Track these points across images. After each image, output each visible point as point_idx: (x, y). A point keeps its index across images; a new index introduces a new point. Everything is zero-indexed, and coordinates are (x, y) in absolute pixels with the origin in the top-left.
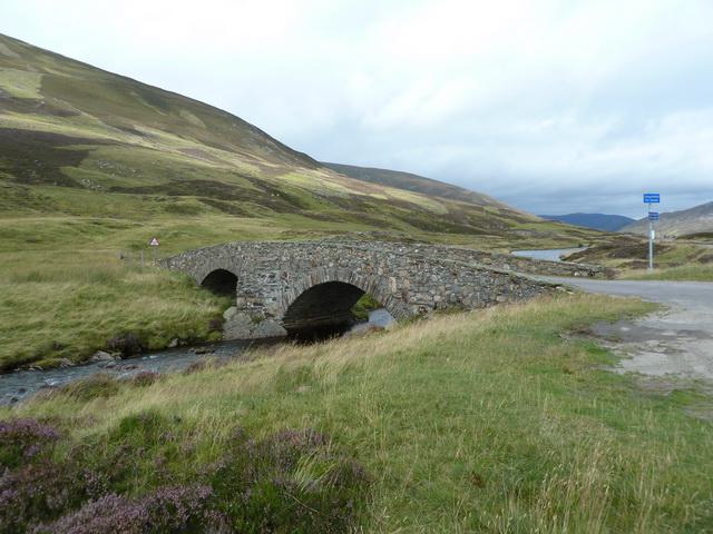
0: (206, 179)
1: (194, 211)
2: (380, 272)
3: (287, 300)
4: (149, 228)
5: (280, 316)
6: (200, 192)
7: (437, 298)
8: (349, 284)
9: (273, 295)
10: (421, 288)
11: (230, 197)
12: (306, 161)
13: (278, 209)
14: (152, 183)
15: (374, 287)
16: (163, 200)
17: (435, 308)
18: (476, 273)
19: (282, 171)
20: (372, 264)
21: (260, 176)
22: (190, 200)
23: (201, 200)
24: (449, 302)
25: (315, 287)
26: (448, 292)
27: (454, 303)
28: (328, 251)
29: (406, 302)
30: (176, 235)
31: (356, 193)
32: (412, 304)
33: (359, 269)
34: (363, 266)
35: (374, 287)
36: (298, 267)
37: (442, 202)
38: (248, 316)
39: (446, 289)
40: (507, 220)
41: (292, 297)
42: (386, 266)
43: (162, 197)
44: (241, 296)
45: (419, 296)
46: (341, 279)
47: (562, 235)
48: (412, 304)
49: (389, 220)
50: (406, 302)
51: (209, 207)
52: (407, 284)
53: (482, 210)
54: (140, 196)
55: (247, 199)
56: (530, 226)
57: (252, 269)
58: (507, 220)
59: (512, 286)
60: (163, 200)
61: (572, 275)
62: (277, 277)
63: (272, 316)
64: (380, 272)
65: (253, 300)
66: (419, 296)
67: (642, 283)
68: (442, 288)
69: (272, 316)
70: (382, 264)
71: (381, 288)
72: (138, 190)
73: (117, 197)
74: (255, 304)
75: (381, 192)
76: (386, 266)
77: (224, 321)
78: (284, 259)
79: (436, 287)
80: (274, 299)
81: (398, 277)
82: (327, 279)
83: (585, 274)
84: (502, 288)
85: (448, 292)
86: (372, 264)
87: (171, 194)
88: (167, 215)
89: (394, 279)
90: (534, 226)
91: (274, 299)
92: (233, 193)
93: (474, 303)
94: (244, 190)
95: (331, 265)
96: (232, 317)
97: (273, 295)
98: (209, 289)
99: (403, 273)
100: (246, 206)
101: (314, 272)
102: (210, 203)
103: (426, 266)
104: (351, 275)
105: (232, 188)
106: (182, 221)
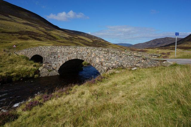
0: (30, 31)
1: (27, 39)
2: (93, 56)
3: (60, 65)
4: (14, 43)
5: (58, 69)
6: (29, 34)
7: (114, 65)
8: (81, 60)
9: (55, 63)
10: (108, 61)
11: (37, 36)
12: (57, 28)
13: (50, 39)
14: (14, 31)
15: (91, 61)
16: (18, 36)
17: (113, 68)
18: (129, 56)
19: (51, 30)
20: (90, 54)
21: (45, 31)
22: (26, 36)
23: (29, 36)
24: (118, 66)
25: (69, 61)
26: (118, 63)
27: (120, 66)
28: (74, 49)
29: (102, 65)
30: (22, 45)
31: (70, 36)
32: (104, 66)
33: (85, 55)
34: (87, 54)
35: (91, 61)
36: (63, 54)
37: (91, 39)
38: (47, 70)
39: (117, 62)
40: (106, 44)
41: (61, 64)
42: (95, 54)
43: (17, 35)
44: (44, 63)
45: (107, 64)
46: (79, 58)
47: (119, 48)
48: (104, 66)
49: (79, 43)
50: (102, 65)
51: (31, 38)
52: (103, 60)
53: (100, 41)
54: (11, 34)
55: (42, 37)
56: (112, 46)
57: (48, 55)
58: (106, 44)
59: (143, 61)
60: (18, 36)
61: (152, 57)
62: (56, 57)
63: (55, 69)
64: (93, 56)
65: (48, 64)
66: (107, 64)
67: (175, 59)
68: (116, 61)
69: (55, 69)
70: (94, 53)
71: (93, 61)
72: (10, 33)
73: (4, 34)
74: (49, 66)
75: (77, 36)
76: (95, 54)
77: (39, 71)
78: (58, 51)
79: (113, 61)
80: (55, 64)
81: (99, 57)
82: (74, 58)
83: (156, 57)
84: (138, 61)
85: (118, 63)
86: (90, 54)
87: (20, 34)
88: (19, 40)
89: (98, 58)
90: (113, 46)
91: (55, 64)
92: (38, 35)
93: (128, 66)
94: (41, 34)
95: (75, 53)
96: (42, 70)
97: (55, 63)
98: (75, 84)
99: (101, 56)
100: (41, 38)
101: (69, 56)
102: (32, 37)
103: (110, 54)
104: (82, 57)
105: (38, 33)
106: (23, 41)
